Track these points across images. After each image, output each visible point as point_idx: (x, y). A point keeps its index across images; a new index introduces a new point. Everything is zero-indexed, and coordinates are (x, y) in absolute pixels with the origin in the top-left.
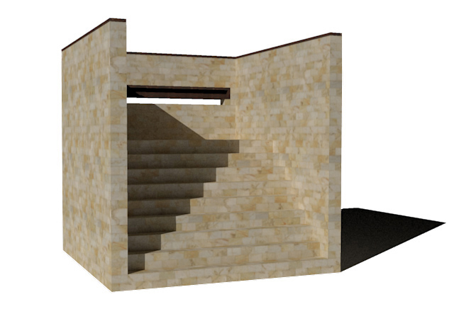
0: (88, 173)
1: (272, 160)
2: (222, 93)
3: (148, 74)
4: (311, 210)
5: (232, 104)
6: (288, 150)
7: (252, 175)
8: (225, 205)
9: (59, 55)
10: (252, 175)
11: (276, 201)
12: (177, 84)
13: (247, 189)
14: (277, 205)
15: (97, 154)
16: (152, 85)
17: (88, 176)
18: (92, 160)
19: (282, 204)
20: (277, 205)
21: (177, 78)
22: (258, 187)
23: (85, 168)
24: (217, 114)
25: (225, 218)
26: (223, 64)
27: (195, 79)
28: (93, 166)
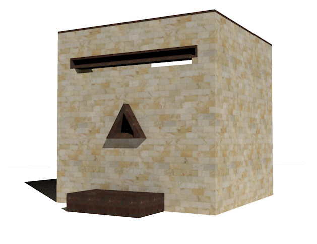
0: (254, 131)
1: (196, 120)
2: (188, 52)
3: (119, 42)
4: (67, 159)
5: (199, 62)
6: (235, 112)
7: (172, 133)
8: (140, 156)
9: (56, 36)
10: (172, 133)
11: (182, 156)
12: (145, 48)
13: (162, 145)
14: (183, 159)
15: (263, 118)
16: (123, 52)
17: (255, 132)
18: (258, 121)
19: (187, 158)
20: (183, 159)
21: (144, 42)
22: (84, 143)
23: (250, 127)
24: (183, 74)
25: (135, 166)
26: (99, 33)
27: (76, 51)
28: (259, 125)
